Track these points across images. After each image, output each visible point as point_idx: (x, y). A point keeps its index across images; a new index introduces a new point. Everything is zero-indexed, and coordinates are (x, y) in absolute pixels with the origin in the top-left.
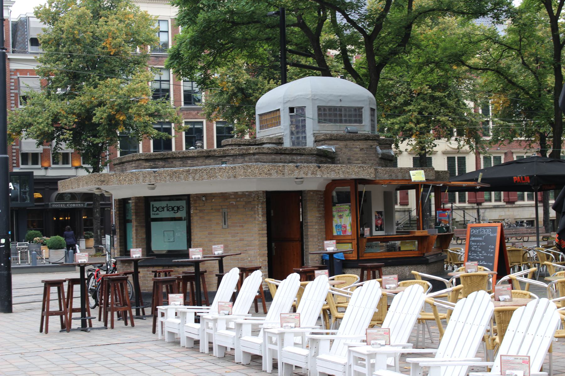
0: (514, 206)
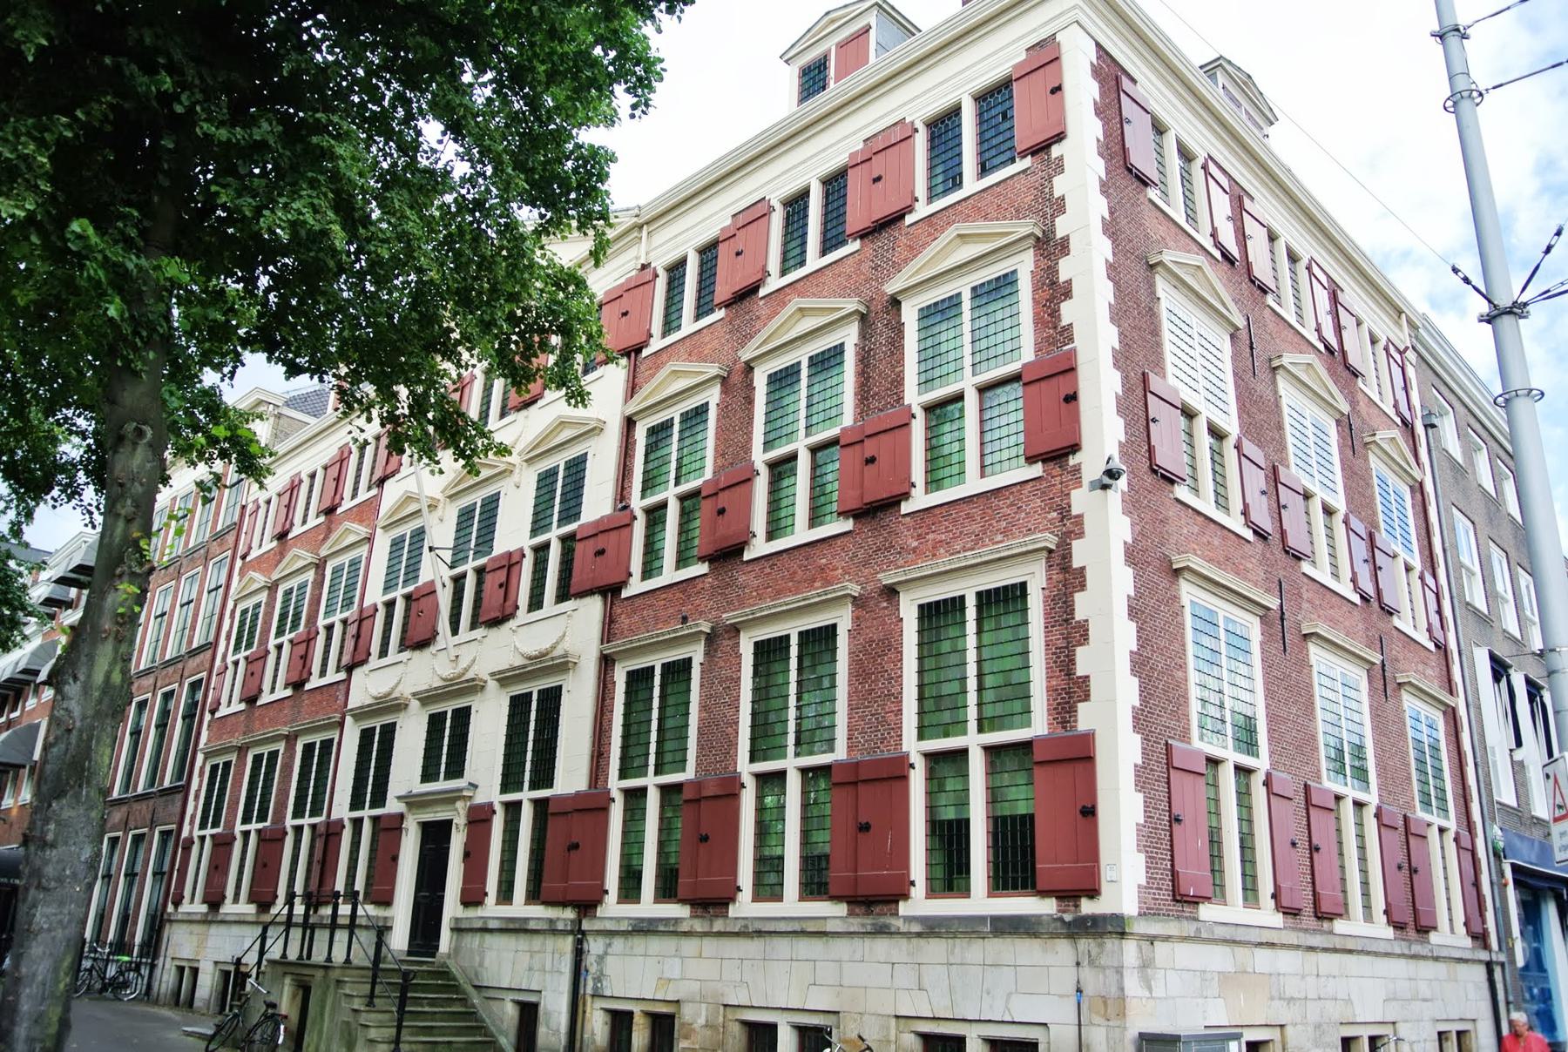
0: (718, 925)
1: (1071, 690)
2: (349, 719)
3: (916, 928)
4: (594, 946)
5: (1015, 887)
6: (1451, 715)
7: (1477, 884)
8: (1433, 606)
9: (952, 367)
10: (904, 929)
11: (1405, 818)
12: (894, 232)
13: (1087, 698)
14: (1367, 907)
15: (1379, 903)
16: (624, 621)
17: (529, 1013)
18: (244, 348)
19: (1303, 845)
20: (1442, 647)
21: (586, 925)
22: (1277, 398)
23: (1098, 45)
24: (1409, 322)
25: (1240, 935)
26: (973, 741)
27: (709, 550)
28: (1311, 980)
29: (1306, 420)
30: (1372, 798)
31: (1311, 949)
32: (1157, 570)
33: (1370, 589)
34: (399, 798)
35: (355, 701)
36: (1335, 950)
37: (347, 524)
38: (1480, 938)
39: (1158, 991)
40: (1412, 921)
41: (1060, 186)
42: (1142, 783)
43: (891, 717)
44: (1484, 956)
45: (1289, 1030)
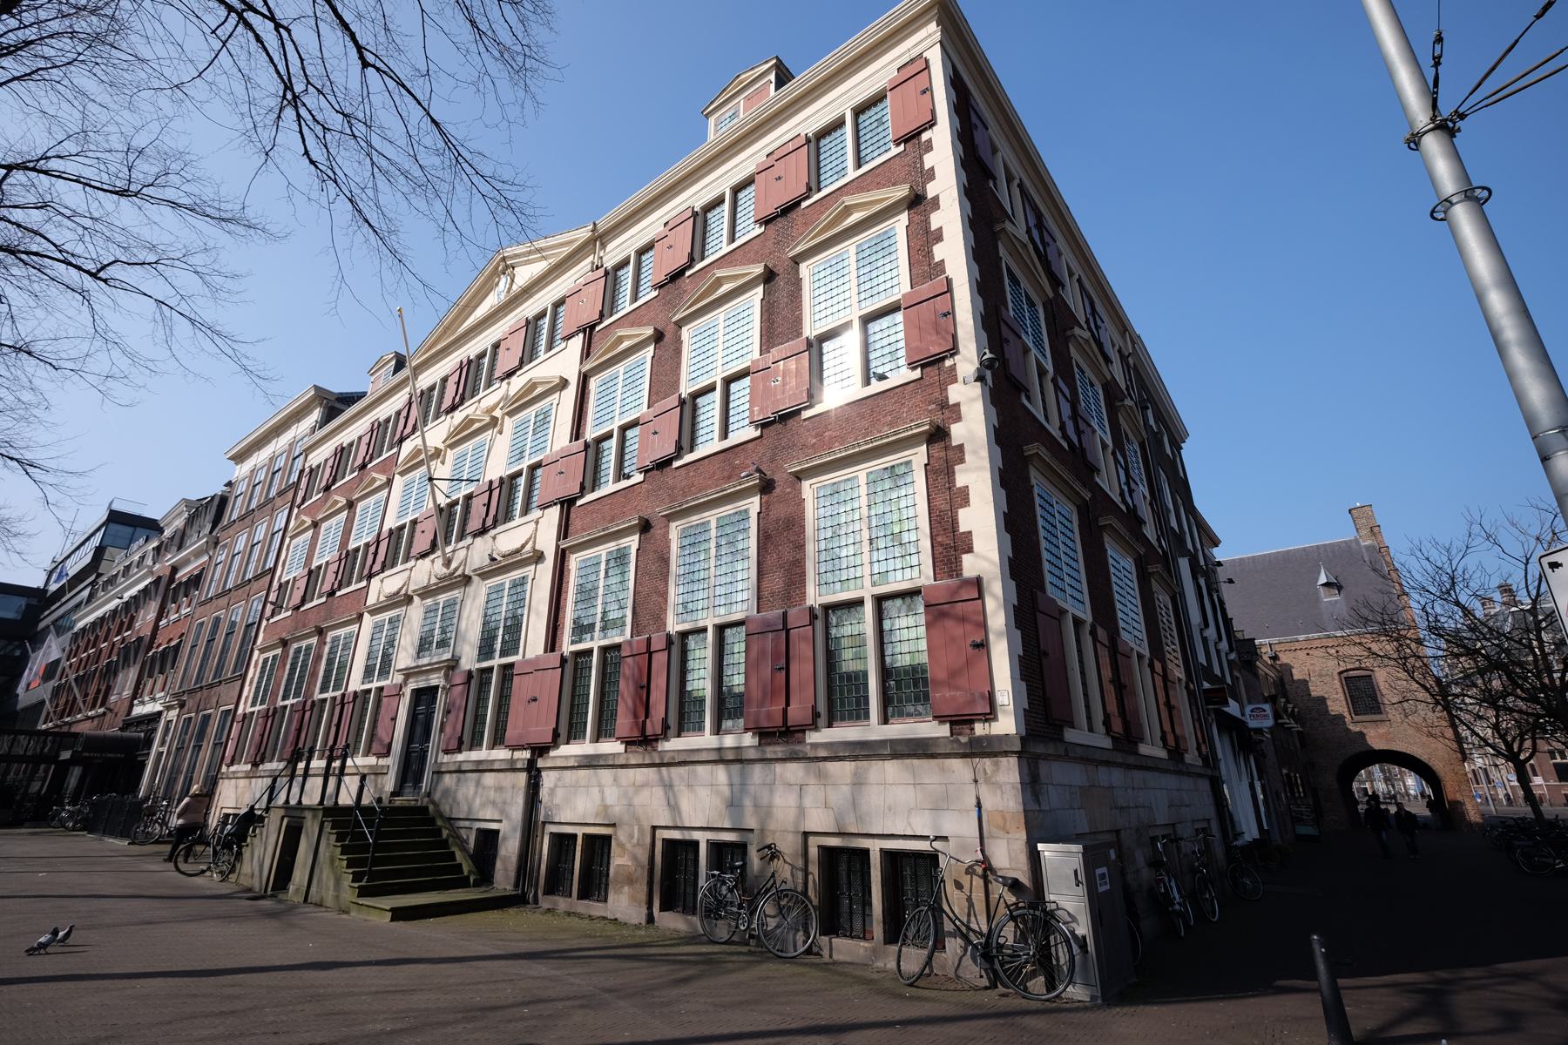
2: (366, 616)
4: (548, 779)
5: (850, 718)
10: (811, 755)
12: (793, 215)
16: (576, 523)
17: (489, 839)
18: (28, 605)
35: (372, 600)
37: (374, 475)
41: (929, 160)
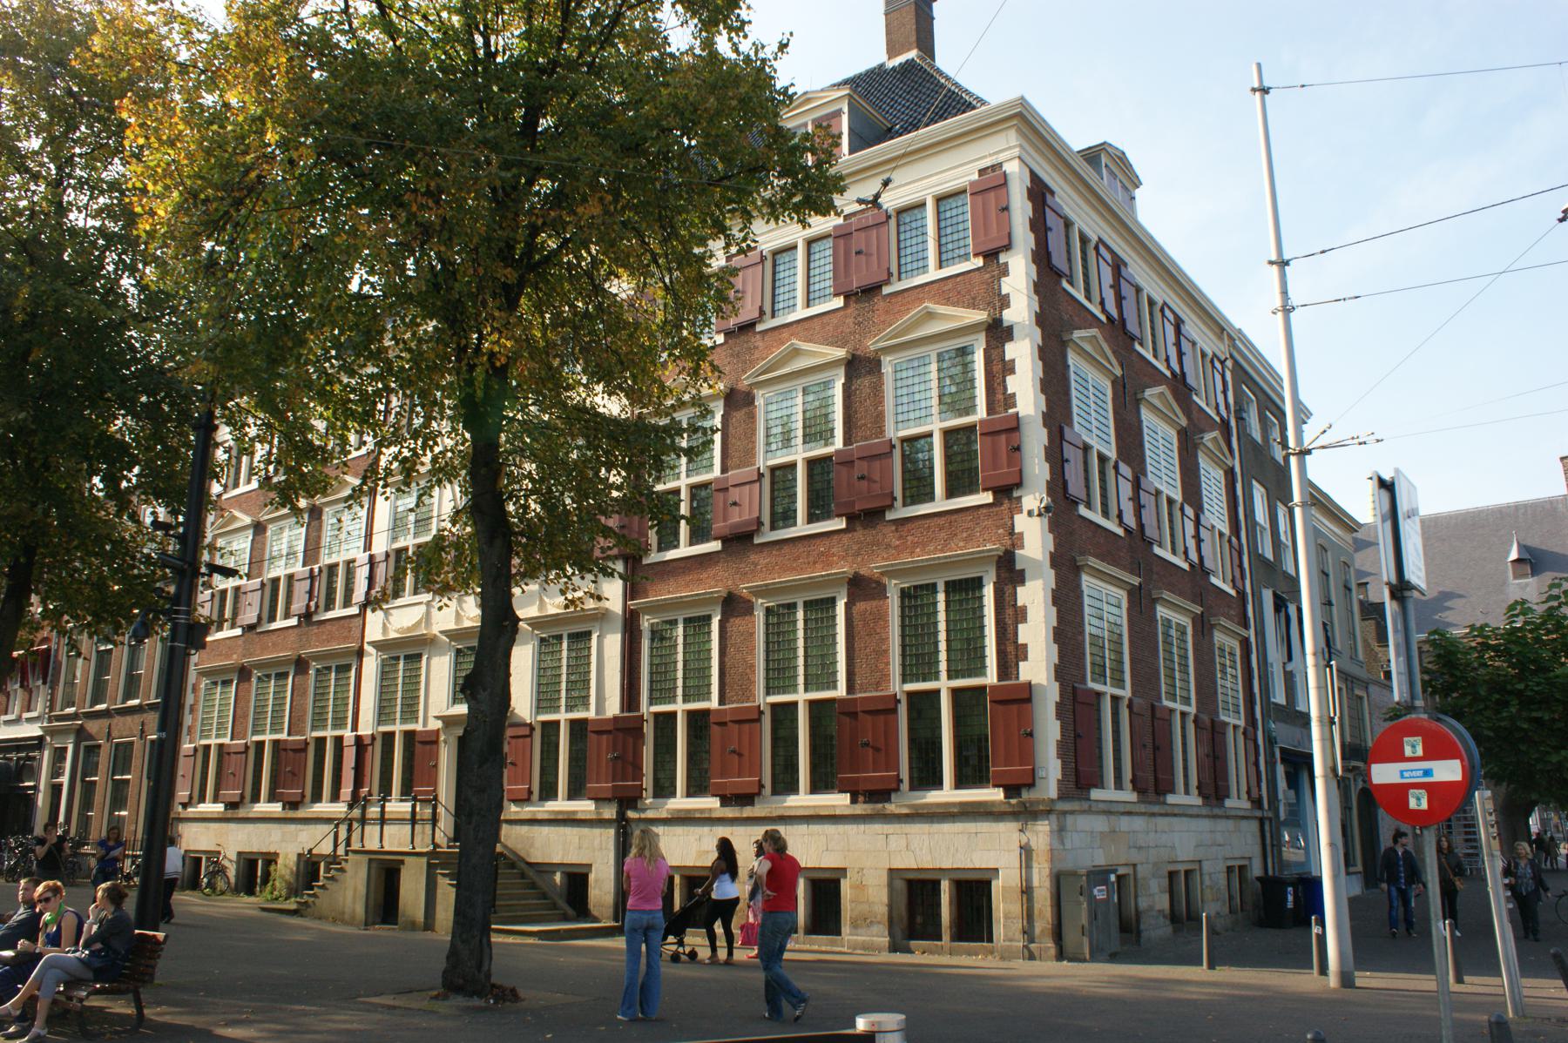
1: (1012, 653)
3: (1445, 844)
6: (1245, 643)
7: (1257, 764)
8: (1236, 562)
9: (923, 413)
11: (1213, 722)
13: (1025, 659)
14: (1186, 785)
15: (1194, 782)
19: (1150, 745)
20: (1242, 594)
21: (631, 814)
22: (1140, 422)
23: (1032, 173)
24: (1230, 336)
25: (1115, 808)
26: (944, 685)
27: (727, 532)
28: (1152, 835)
29: (1159, 436)
30: (1192, 709)
31: (1153, 815)
32: (1066, 565)
33: (1114, 313)
34: (437, 718)
36: (1166, 815)
38: (1257, 803)
39: (1068, 846)
40: (1214, 790)
42: (1060, 715)
43: (882, 666)
44: (1258, 813)
45: (1139, 868)
